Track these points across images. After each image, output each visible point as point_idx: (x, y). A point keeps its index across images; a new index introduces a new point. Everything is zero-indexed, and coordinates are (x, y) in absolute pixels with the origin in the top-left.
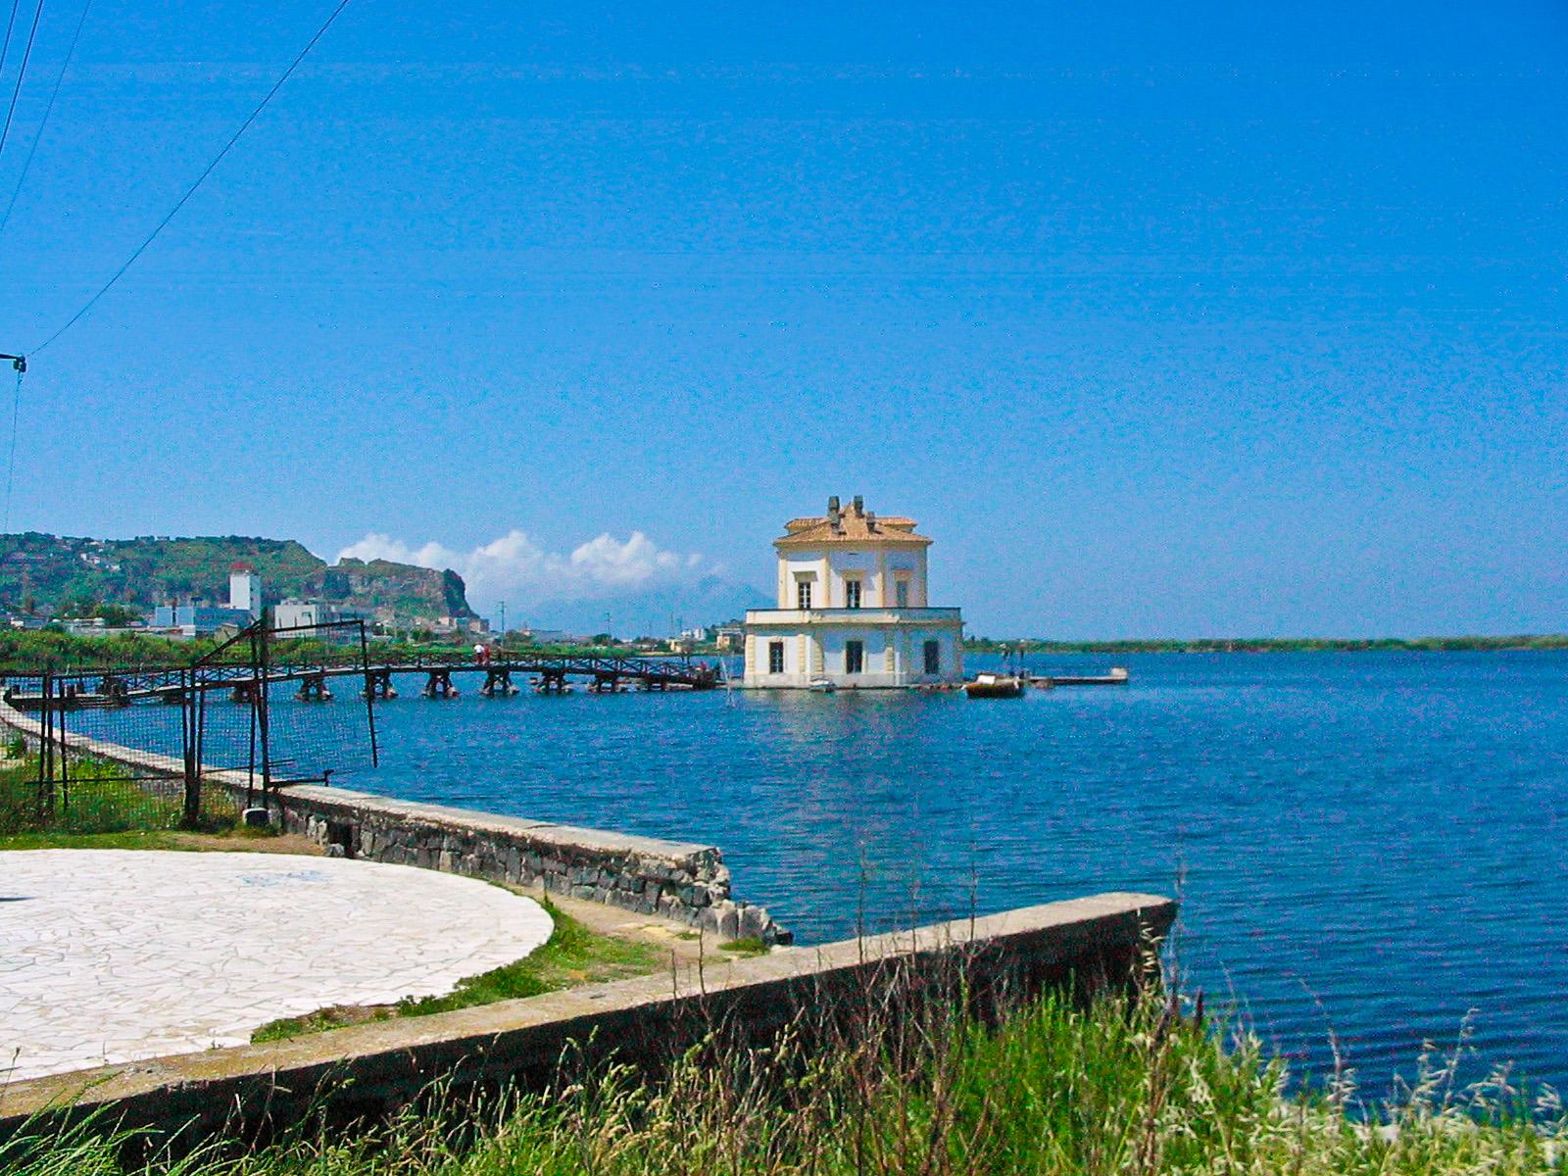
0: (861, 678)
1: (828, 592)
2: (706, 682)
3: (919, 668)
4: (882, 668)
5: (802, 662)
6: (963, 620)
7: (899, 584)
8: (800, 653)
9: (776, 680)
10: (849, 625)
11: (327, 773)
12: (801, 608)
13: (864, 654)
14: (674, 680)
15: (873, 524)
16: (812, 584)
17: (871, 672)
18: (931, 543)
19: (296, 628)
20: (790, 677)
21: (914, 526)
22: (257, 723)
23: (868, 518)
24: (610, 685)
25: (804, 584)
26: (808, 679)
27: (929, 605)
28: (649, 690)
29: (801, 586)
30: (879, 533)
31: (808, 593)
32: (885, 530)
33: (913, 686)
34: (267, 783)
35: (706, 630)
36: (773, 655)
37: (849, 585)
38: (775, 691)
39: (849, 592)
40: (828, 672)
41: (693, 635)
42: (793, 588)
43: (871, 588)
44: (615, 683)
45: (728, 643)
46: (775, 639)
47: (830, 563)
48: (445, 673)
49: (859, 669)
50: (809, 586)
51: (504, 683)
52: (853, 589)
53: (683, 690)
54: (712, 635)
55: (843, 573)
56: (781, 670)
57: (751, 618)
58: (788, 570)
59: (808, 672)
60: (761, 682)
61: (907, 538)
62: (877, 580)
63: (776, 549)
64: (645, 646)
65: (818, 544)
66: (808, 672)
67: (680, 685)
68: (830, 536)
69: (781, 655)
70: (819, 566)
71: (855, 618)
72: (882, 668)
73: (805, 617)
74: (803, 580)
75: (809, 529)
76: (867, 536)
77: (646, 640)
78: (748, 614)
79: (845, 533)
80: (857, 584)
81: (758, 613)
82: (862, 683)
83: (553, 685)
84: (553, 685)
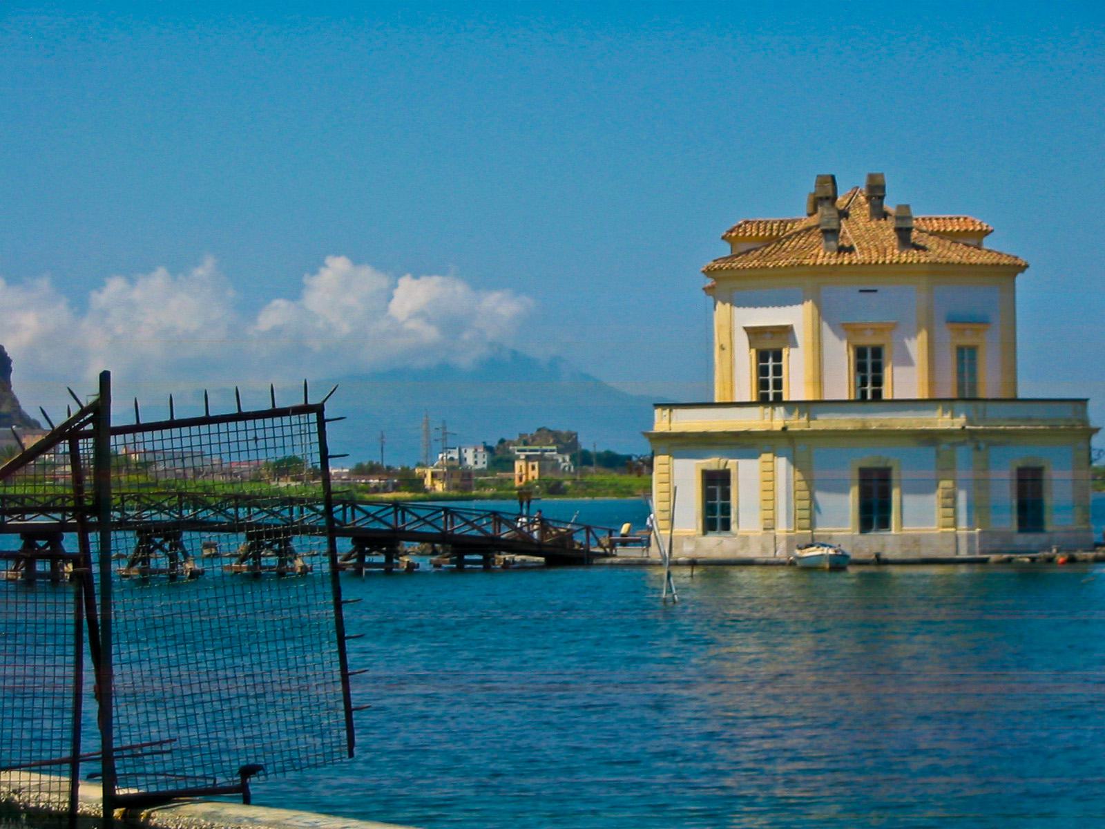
0: (889, 542)
1: (816, 367)
2: (562, 555)
3: (1008, 522)
4: (929, 521)
5: (766, 501)
6: (1094, 423)
7: (960, 350)
8: (760, 485)
9: (716, 546)
10: (862, 434)
11: (248, 771)
12: (763, 401)
13: (895, 494)
14: (510, 546)
15: (909, 230)
16: (785, 352)
17: (910, 529)
18: (1022, 268)
19: (172, 424)
20: (745, 539)
21: (987, 233)
22: (86, 647)
23: (897, 218)
24: (381, 559)
25: (769, 349)
26: (782, 545)
27: (1020, 396)
28: (460, 568)
29: (762, 356)
30: (918, 248)
31: (778, 370)
32: (931, 243)
33: (993, 557)
34: (110, 801)
35: (489, 449)
36: (708, 495)
37: (860, 353)
38: (715, 570)
39: (860, 368)
40: (821, 530)
41: (462, 460)
42: (745, 360)
43: (906, 361)
44: (392, 553)
45: (534, 474)
46: (713, 463)
47: (823, 313)
48: (172, 532)
49: (885, 524)
50: (778, 356)
51: (173, 557)
52: (869, 365)
53: (524, 567)
54: (501, 459)
55: (846, 329)
56: (726, 526)
57: (663, 422)
58: (734, 322)
59: (782, 529)
60: (686, 551)
61: (976, 258)
62: (917, 346)
63: (709, 282)
64: (374, 481)
65: (798, 269)
66: (782, 529)
67: (518, 558)
68: (823, 255)
69: (726, 495)
70: (797, 316)
71: (877, 420)
72: (929, 521)
73: (776, 419)
74: (769, 344)
75: (774, 240)
76: (895, 254)
77: (373, 470)
78: (658, 412)
79: (851, 250)
80: (877, 352)
81: (678, 412)
82: (890, 553)
83: (270, 560)
84: (160, 561)
